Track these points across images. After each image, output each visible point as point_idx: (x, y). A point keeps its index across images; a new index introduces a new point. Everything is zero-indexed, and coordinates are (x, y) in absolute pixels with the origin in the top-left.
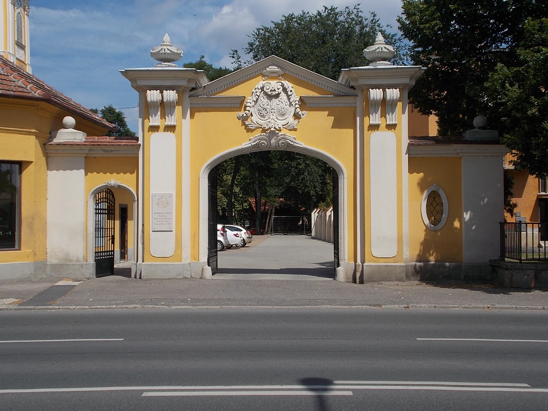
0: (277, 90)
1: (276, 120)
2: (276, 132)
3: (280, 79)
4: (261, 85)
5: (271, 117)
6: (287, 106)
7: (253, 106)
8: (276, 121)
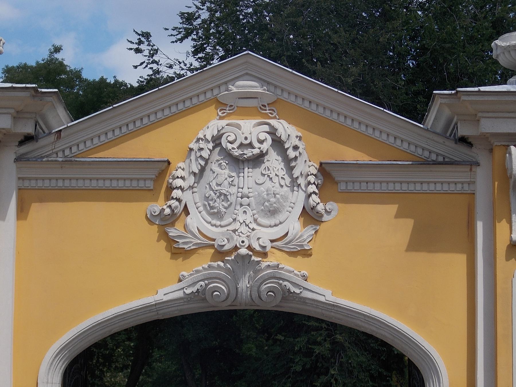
0: (256, 144)
1: (253, 225)
2: (254, 258)
3: (266, 114)
4: (213, 130)
5: (241, 218)
6: (285, 188)
7: (191, 187)
8: (253, 230)
